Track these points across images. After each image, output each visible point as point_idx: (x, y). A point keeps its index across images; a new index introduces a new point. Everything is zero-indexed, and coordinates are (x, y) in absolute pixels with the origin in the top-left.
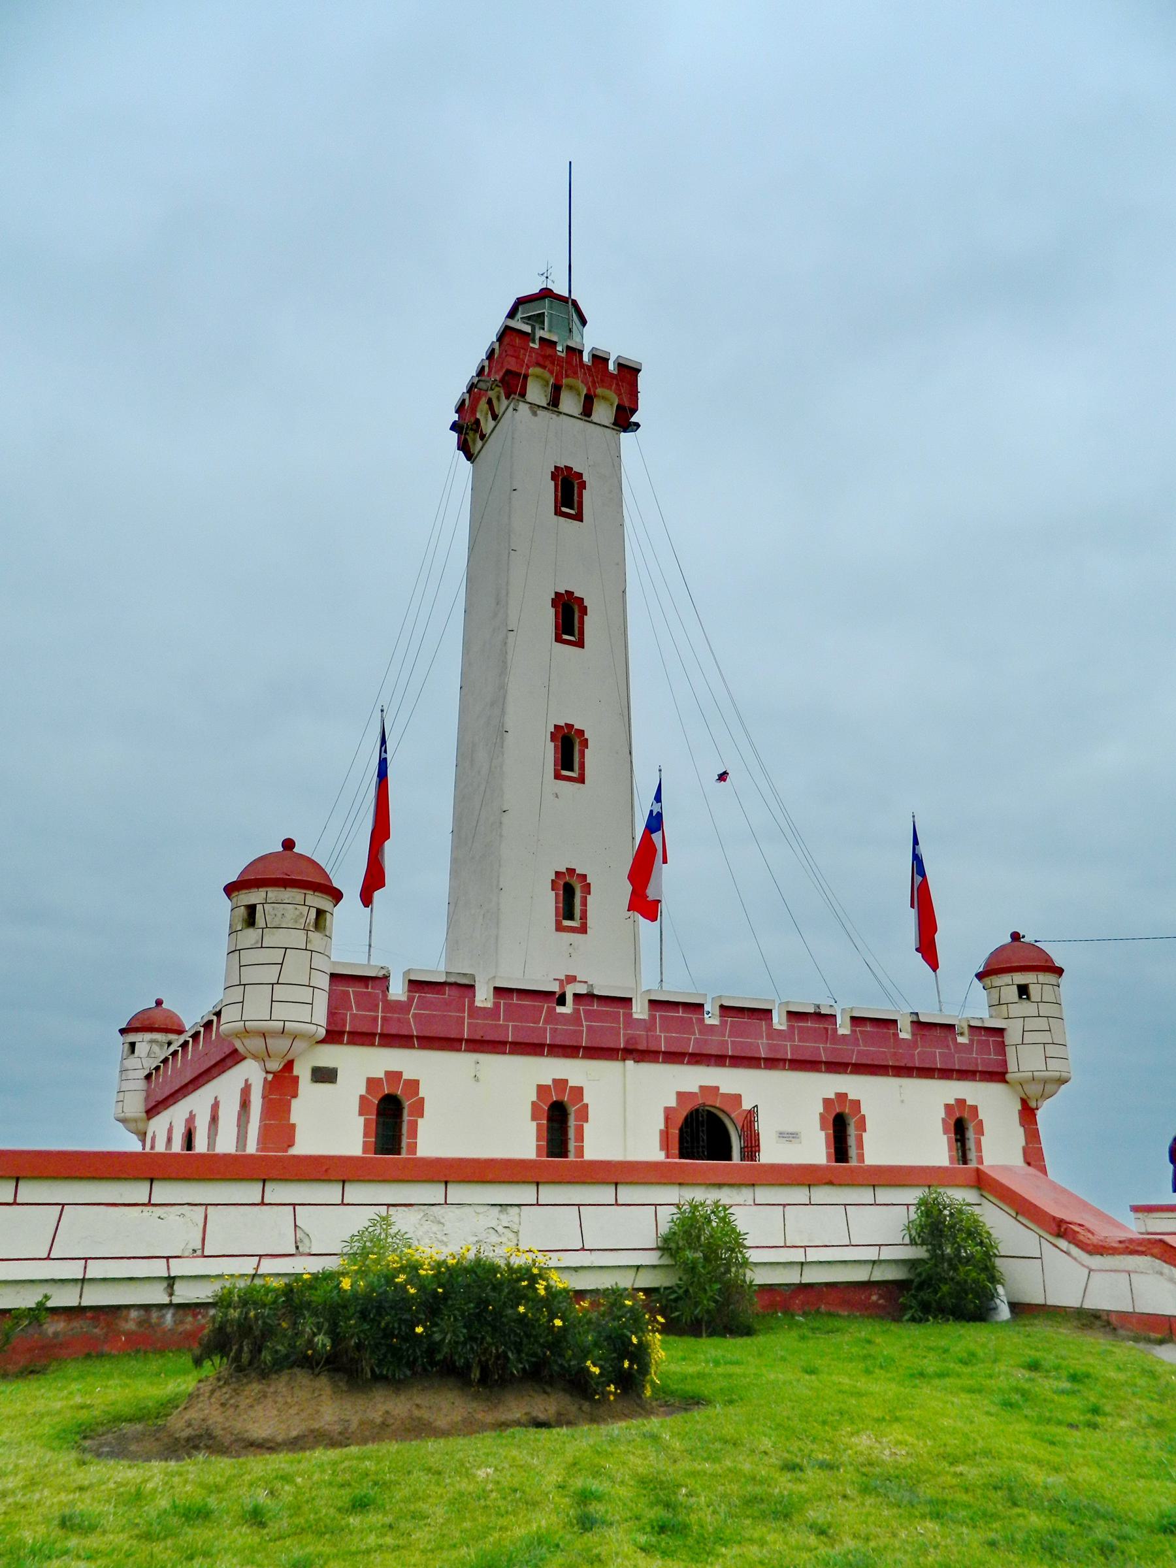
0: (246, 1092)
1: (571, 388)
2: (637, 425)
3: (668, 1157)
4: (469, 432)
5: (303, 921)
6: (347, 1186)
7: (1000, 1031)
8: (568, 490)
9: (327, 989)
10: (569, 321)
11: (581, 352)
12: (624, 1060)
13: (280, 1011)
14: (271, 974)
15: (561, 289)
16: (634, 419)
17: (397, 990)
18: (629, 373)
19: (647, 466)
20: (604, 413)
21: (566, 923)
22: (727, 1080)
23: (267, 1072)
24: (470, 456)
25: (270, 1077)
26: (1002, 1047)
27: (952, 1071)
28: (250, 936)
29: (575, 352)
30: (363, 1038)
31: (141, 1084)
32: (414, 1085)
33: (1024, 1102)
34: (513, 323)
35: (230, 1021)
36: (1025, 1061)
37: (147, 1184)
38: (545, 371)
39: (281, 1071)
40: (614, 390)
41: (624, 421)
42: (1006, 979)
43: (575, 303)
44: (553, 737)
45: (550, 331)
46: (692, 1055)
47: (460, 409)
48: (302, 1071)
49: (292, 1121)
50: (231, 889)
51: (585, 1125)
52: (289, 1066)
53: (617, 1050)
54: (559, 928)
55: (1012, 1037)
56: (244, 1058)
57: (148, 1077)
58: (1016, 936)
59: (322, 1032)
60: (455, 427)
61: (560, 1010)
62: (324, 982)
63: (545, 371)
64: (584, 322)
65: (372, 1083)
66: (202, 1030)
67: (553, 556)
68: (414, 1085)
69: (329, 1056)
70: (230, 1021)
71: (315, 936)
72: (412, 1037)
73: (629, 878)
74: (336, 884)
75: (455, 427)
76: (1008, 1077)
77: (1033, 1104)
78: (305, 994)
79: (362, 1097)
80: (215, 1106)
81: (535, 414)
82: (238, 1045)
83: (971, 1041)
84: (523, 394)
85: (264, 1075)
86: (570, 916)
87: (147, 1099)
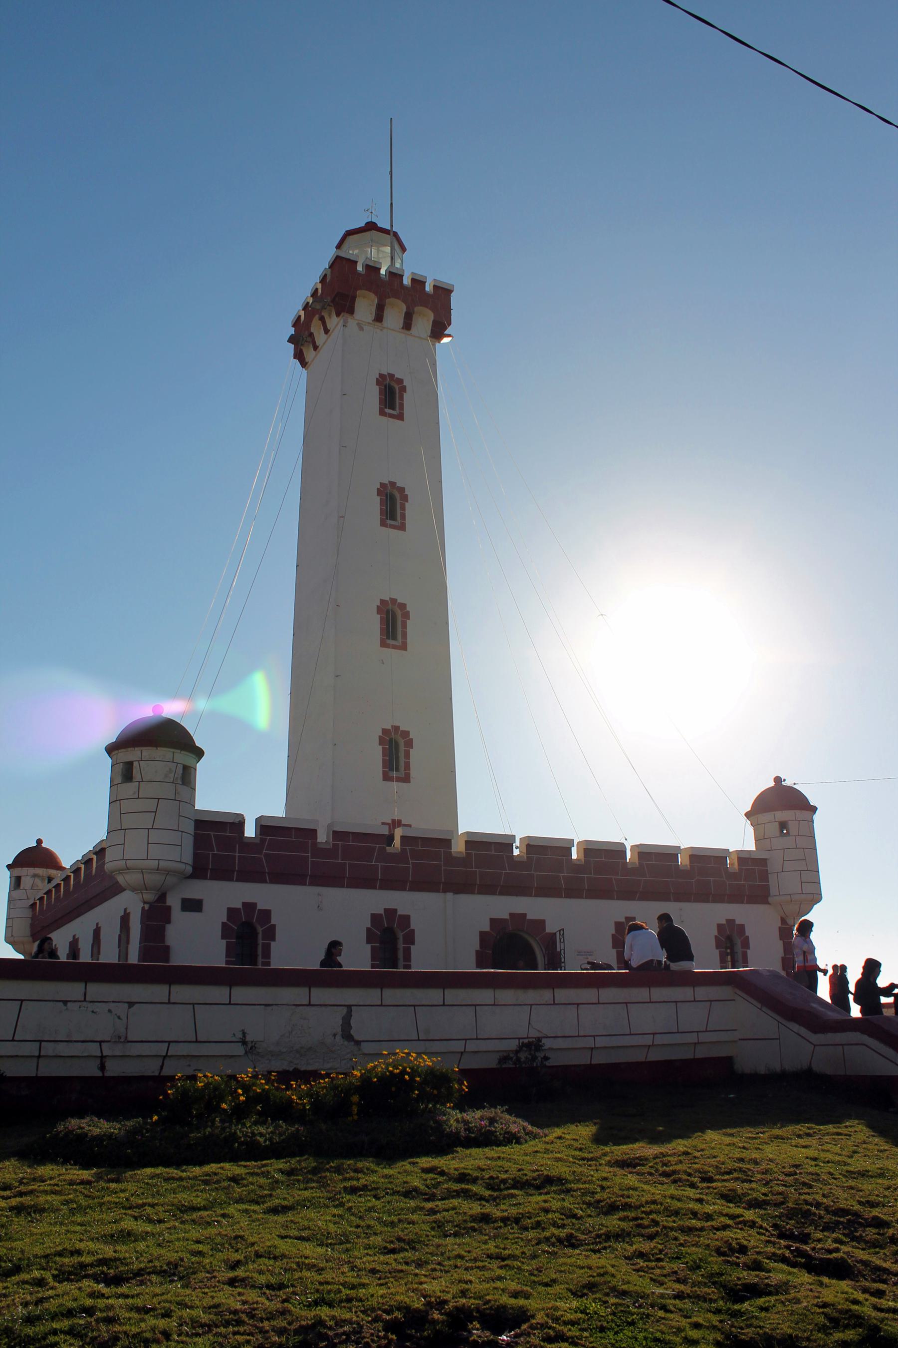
0: (125, 920)
4: (302, 340)
6: (556, 990)
8: (391, 394)
11: (401, 276)
18: (443, 294)
20: (423, 322)
22: (533, 907)
23: (145, 903)
24: (304, 364)
25: (147, 907)
26: (764, 876)
28: (131, 787)
29: (395, 276)
30: (223, 873)
31: (28, 913)
34: (342, 254)
37: (442, 990)
39: (155, 902)
40: (430, 307)
47: (296, 323)
48: (174, 901)
49: (368, 947)
52: (162, 897)
57: (33, 906)
58: (778, 780)
59: (189, 869)
60: (291, 340)
62: (190, 828)
64: (404, 249)
66: (83, 866)
69: (198, 889)
70: (112, 861)
71: (183, 790)
75: (291, 340)
76: (770, 899)
79: (223, 924)
80: (97, 932)
81: (361, 329)
82: (120, 879)
85: (142, 905)
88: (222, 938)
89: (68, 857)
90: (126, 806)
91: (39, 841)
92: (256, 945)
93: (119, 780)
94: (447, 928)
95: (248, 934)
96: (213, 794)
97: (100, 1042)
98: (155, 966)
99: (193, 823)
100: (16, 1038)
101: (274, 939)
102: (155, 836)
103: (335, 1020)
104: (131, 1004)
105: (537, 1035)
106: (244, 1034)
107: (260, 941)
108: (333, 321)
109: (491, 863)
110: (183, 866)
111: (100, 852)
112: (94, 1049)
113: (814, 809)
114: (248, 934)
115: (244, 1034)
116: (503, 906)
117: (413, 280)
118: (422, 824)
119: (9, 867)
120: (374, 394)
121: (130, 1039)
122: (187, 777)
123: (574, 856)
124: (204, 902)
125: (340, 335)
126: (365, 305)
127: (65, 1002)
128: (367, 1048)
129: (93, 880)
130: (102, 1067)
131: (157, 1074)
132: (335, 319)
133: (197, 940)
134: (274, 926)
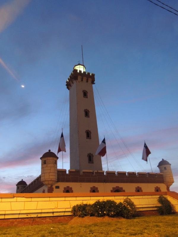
2: (95, 83)
3: (161, 172)
7: (162, 175)
8: (85, 94)
16: (94, 82)
18: (93, 75)
20: (90, 80)
24: (69, 89)
28: (45, 165)
30: (63, 181)
41: (93, 82)
48: (54, 187)
52: (52, 186)
58: (163, 159)
59: (57, 180)
60: (66, 85)
61: (93, 175)
62: (56, 172)
69: (59, 184)
73: (106, 153)
75: (66, 85)
82: (44, 183)
91: (22, 180)
102: (51, 174)
104: (56, 208)
108: (74, 81)
111: (40, 177)
113: (170, 165)
117: (92, 74)
119: (16, 185)
123: (127, 175)
124: (58, 189)
125: (74, 85)
126: (79, 78)
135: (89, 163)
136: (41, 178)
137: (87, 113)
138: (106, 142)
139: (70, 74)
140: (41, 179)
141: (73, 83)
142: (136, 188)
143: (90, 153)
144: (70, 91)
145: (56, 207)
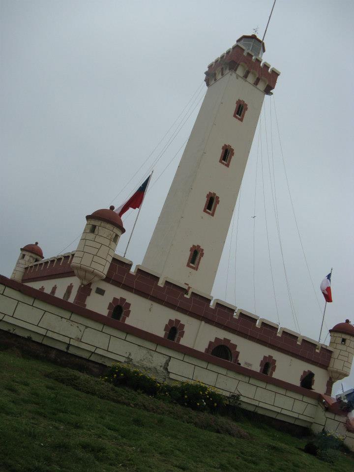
0: (70, 288)
1: (253, 73)
2: (272, 94)
4: (211, 76)
5: (110, 237)
7: (331, 352)
8: (240, 110)
9: (110, 262)
10: (260, 49)
11: (261, 62)
12: (202, 320)
13: (94, 266)
14: (94, 251)
15: (260, 37)
16: (271, 91)
17: (161, 283)
18: (275, 74)
19: (272, 109)
20: (262, 86)
21: (191, 265)
22: (234, 339)
24: (208, 85)
25: (83, 286)
26: (329, 358)
27: (290, 352)
28: (91, 236)
29: (259, 61)
30: (117, 283)
31: (23, 270)
32: (183, 326)
33: (330, 378)
34: (240, 45)
35: (75, 262)
36: (336, 365)
38: (245, 66)
40: (267, 79)
41: (268, 90)
42: (339, 335)
43: (263, 44)
44: (208, 196)
45: (251, 51)
46: (279, 348)
48: (94, 288)
50: (88, 218)
51: (127, 318)
52: (90, 284)
53: (200, 316)
54: (188, 265)
55: (335, 355)
56: (75, 276)
57: (26, 268)
58: (347, 321)
59: (105, 276)
61: (185, 296)
62: (110, 259)
63: (245, 66)
64: (264, 51)
65: (115, 299)
67: (228, 131)
68: (183, 326)
69: (104, 286)
70: (75, 262)
71: (113, 243)
72: (133, 288)
74: (124, 226)
77: (333, 380)
78: (103, 262)
82: (76, 271)
83: (320, 352)
84: (236, 70)
86: (193, 262)
87: (23, 276)
88: (108, 309)
89: (48, 255)
90: (88, 243)
91: (37, 243)
92: (120, 316)
93: (88, 231)
94: (199, 335)
95: (119, 310)
96: (121, 250)
97: (71, 338)
98: (78, 309)
99: (111, 259)
100: (39, 325)
101: (128, 316)
103: (163, 360)
104: (87, 327)
105: (238, 393)
106: (130, 354)
107: (123, 315)
109: (222, 316)
110: (103, 274)
112: (67, 340)
114: (119, 310)
115: (130, 354)
116: (223, 334)
118: (197, 287)
120: (233, 107)
121: (82, 341)
122: (116, 239)
127: (62, 318)
128: (172, 376)
129: (62, 267)
130: (68, 348)
131: (87, 358)
132: (228, 71)
133: (99, 304)
134: (130, 311)
135: (188, 265)
136: (74, 258)
137: (227, 154)
138: (332, 278)
139: (225, 51)
140: (73, 261)
141: (222, 74)
142: (265, 357)
143: (199, 246)
144: (208, 92)
145: (80, 337)
